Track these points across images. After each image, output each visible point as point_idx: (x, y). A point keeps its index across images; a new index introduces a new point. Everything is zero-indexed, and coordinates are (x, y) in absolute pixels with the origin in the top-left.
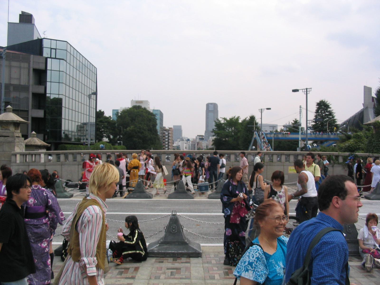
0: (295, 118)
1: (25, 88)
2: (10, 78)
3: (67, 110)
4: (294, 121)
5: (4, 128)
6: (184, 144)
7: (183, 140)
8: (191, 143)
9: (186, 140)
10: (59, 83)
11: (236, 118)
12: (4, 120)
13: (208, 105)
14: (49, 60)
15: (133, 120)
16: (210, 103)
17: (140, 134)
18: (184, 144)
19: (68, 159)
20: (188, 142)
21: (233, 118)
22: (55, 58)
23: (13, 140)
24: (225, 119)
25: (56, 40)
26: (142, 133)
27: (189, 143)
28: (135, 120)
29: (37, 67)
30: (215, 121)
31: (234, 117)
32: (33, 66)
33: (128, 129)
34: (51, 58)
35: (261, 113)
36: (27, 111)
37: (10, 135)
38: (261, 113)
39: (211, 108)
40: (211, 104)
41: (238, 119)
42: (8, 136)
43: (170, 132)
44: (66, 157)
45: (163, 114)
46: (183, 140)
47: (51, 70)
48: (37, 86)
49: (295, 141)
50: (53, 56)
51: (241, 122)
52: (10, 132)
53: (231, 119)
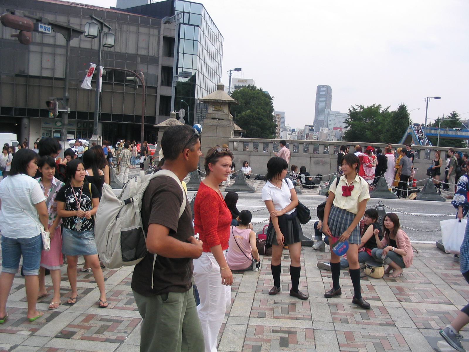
0: (453, 111)
1: (154, 60)
2: (137, 48)
3: (199, 87)
4: (451, 114)
5: (216, 109)
6: (288, 134)
7: (286, 130)
8: (297, 134)
9: (290, 131)
10: (193, 55)
11: (376, 106)
12: (219, 100)
13: (319, 88)
14: (182, 26)
15: (247, 103)
16: (322, 86)
17: (258, 121)
18: (288, 134)
19: (257, 148)
20: (294, 133)
21: (373, 107)
22: (189, 24)
23: (228, 123)
24: (361, 107)
25: (190, 2)
26: (261, 119)
27: (294, 135)
28: (249, 103)
29: (168, 35)
30: (349, 109)
31: (374, 105)
32: (163, 33)
33: (243, 114)
34: (183, 23)
35: (427, 102)
36: (156, 88)
37: (224, 117)
38: (426, 103)
39: (323, 92)
40: (323, 86)
41: (379, 107)
42: (223, 119)
43: (277, 120)
44: (256, 147)
45: (270, 98)
46: (286, 130)
47: (184, 39)
48: (168, 58)
49: (451, 140)
50: (186, 21)
51: (382, 112)
52: (224, 114)
53: (370, 108)
